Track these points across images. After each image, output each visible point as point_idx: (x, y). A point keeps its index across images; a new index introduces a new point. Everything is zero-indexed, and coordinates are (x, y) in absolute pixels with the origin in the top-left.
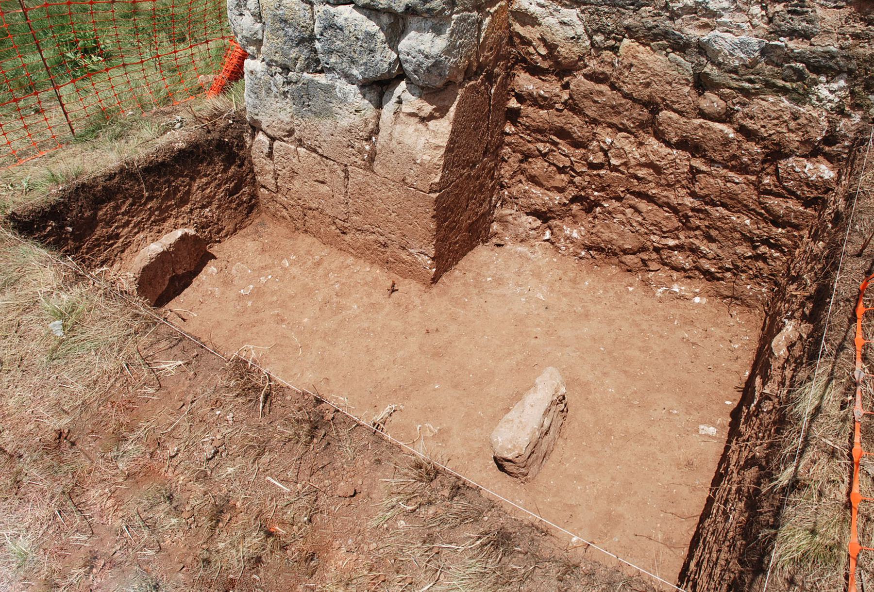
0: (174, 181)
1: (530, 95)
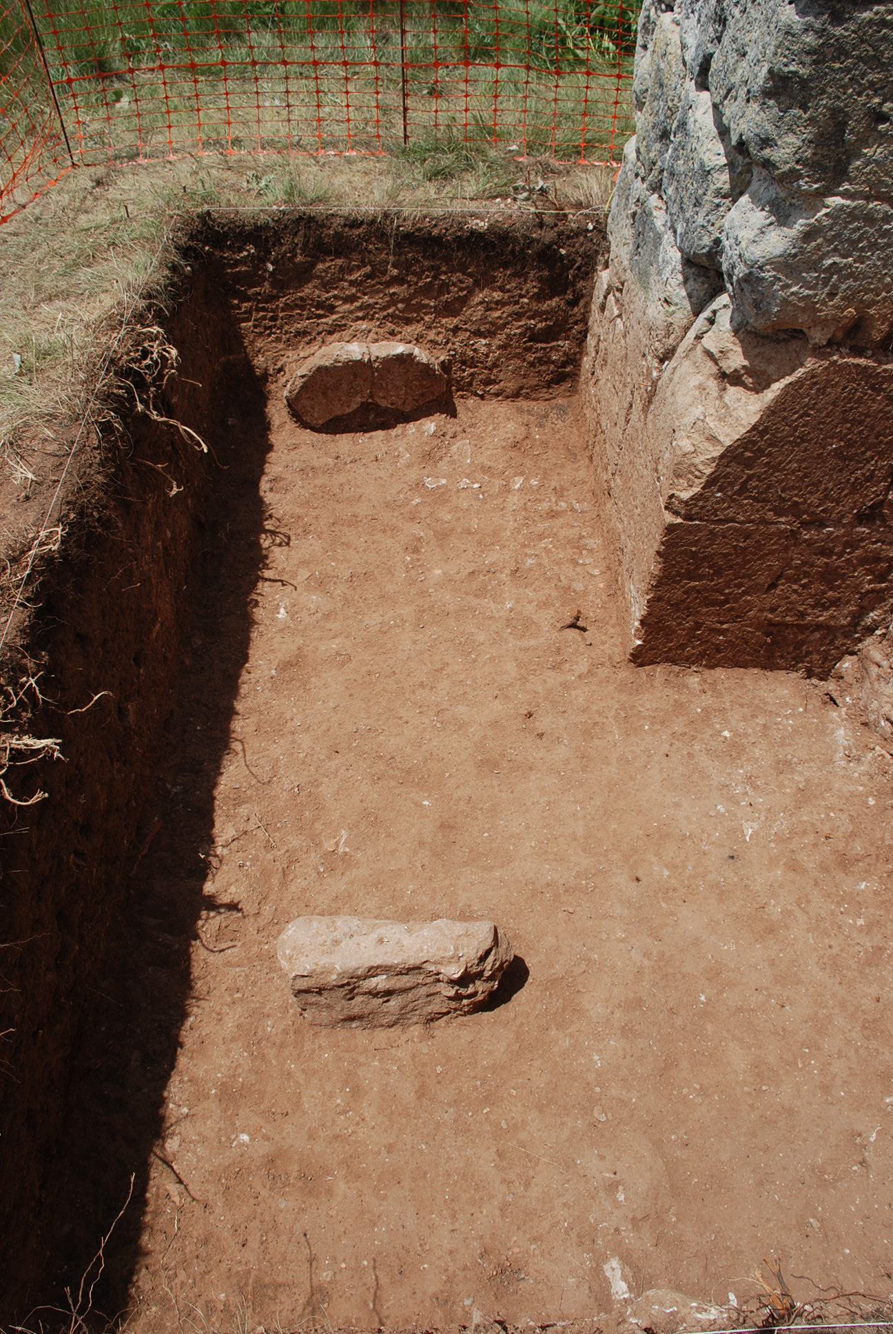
0: (445, 273)
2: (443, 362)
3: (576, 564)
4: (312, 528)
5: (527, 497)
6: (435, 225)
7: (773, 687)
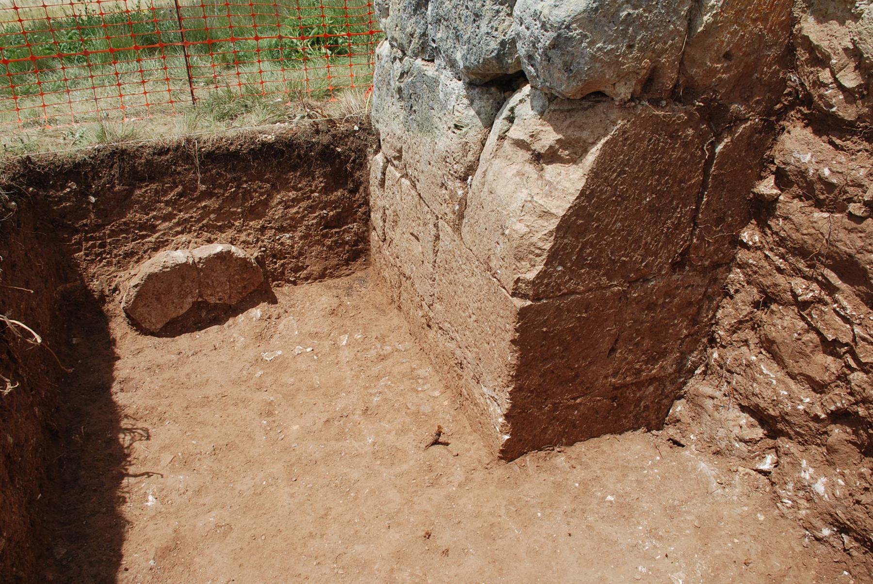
0: (246, 182)
1: (802, 173)
2: (257, 258)
3: (417, 391)
4: (166, 415)
5: (356, 350)
6: (231, 144)
7: (626, 446)
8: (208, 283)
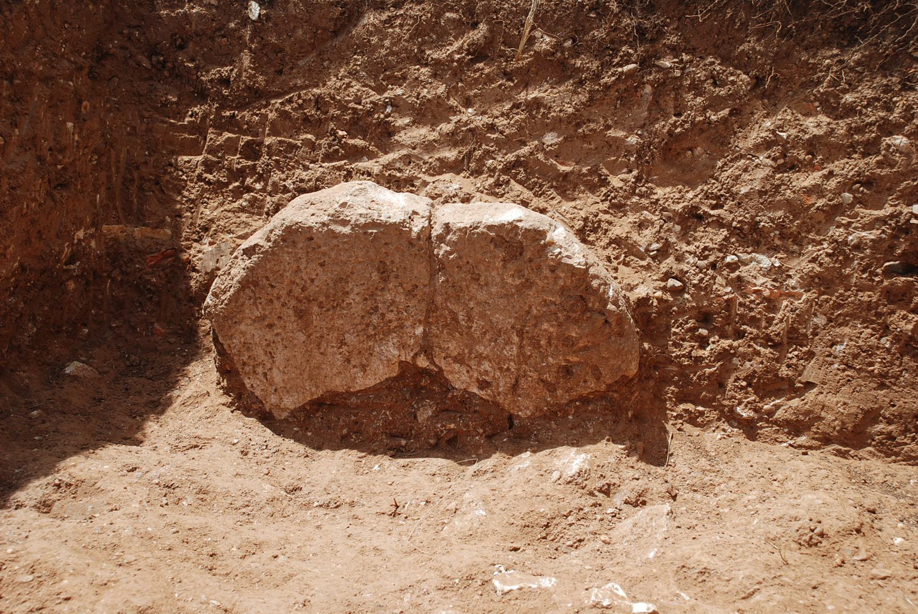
0: (675, 50)
2: (643, 302)
8: (455, 319)
